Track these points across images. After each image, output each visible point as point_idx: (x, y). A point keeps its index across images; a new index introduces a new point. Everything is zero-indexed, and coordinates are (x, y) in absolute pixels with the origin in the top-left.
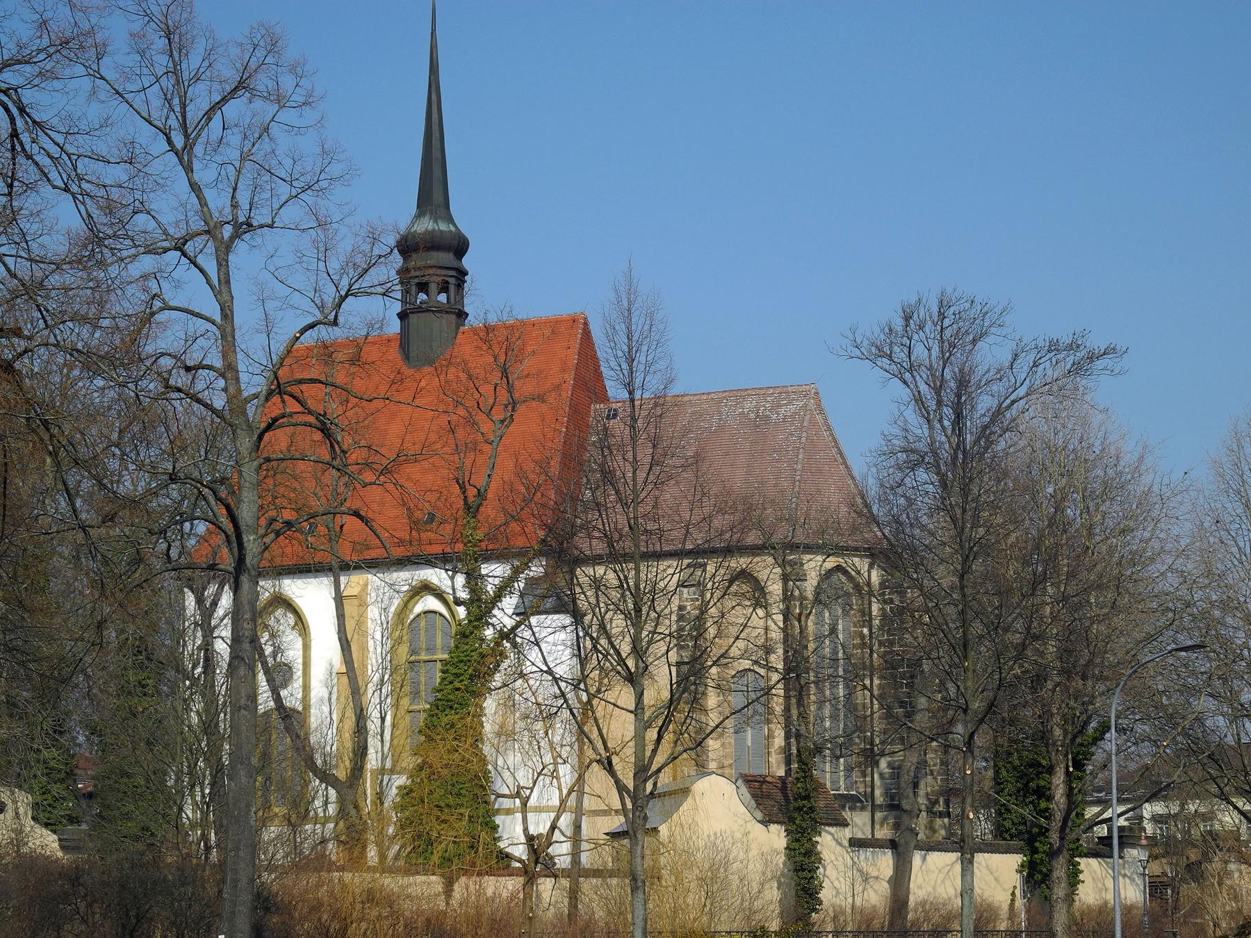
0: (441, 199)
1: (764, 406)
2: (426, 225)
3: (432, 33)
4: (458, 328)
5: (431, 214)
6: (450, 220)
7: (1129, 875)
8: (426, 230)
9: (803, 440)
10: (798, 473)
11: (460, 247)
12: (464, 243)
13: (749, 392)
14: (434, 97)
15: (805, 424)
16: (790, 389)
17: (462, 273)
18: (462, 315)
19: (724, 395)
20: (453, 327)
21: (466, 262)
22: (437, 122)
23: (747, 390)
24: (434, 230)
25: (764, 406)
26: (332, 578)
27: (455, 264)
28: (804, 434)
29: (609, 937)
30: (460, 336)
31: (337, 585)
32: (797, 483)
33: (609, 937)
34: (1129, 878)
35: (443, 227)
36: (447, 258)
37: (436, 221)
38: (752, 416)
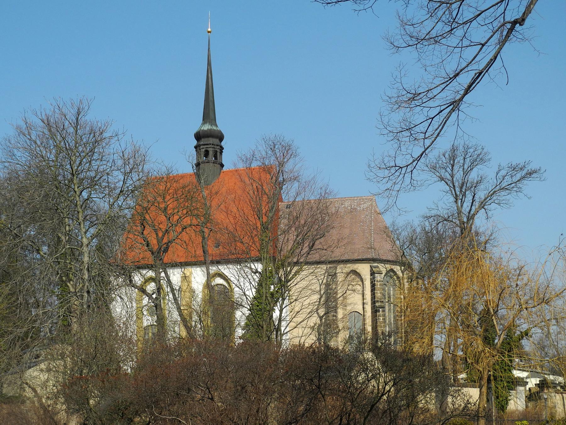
0: (213, 117)
1: (354, 204)
2: (207, 127)
3: (208, 49)
4: (221, 171)
5: (209, 122)
6: (217, 126)
7: (519, 397)
8: (208, 129)
9: (373, 218)
10: (372, 231)
11: (221, 137)
12: (222, 138)
13: (347, 199)
14: (210, 75)
15: (373, 211)
16: (364, 198)
17: (222, 148)
18: (222, 166)
19: (336, 199)
20: (219, 170)
21: (223, 144)
22: (211, 85)
23: (345, 198)
24: (211, 129)
25: (354, 204)
26: (205, 268)
27: (219, 143)
28: (373, 215)
29: (255, 424)
30: (222, 174)
31: (208, 270)
32: (372, 235)
33: (255, 424)
34: (519, 399)
35: (215, 128)
36: (216, 141)
37: (211, 125)
38: (349, 208)
